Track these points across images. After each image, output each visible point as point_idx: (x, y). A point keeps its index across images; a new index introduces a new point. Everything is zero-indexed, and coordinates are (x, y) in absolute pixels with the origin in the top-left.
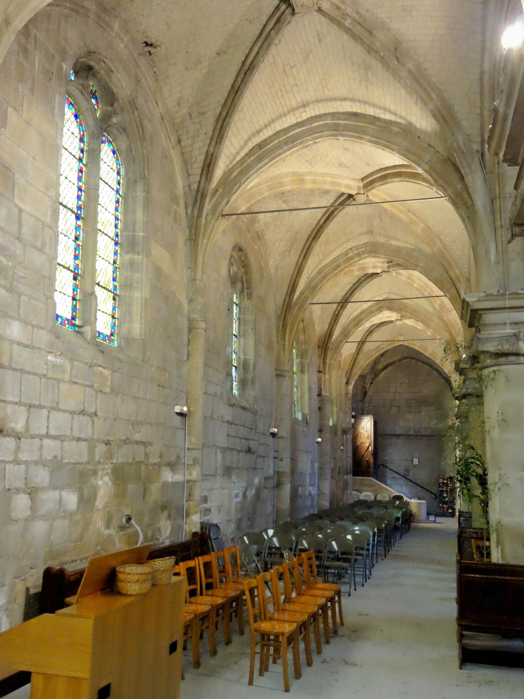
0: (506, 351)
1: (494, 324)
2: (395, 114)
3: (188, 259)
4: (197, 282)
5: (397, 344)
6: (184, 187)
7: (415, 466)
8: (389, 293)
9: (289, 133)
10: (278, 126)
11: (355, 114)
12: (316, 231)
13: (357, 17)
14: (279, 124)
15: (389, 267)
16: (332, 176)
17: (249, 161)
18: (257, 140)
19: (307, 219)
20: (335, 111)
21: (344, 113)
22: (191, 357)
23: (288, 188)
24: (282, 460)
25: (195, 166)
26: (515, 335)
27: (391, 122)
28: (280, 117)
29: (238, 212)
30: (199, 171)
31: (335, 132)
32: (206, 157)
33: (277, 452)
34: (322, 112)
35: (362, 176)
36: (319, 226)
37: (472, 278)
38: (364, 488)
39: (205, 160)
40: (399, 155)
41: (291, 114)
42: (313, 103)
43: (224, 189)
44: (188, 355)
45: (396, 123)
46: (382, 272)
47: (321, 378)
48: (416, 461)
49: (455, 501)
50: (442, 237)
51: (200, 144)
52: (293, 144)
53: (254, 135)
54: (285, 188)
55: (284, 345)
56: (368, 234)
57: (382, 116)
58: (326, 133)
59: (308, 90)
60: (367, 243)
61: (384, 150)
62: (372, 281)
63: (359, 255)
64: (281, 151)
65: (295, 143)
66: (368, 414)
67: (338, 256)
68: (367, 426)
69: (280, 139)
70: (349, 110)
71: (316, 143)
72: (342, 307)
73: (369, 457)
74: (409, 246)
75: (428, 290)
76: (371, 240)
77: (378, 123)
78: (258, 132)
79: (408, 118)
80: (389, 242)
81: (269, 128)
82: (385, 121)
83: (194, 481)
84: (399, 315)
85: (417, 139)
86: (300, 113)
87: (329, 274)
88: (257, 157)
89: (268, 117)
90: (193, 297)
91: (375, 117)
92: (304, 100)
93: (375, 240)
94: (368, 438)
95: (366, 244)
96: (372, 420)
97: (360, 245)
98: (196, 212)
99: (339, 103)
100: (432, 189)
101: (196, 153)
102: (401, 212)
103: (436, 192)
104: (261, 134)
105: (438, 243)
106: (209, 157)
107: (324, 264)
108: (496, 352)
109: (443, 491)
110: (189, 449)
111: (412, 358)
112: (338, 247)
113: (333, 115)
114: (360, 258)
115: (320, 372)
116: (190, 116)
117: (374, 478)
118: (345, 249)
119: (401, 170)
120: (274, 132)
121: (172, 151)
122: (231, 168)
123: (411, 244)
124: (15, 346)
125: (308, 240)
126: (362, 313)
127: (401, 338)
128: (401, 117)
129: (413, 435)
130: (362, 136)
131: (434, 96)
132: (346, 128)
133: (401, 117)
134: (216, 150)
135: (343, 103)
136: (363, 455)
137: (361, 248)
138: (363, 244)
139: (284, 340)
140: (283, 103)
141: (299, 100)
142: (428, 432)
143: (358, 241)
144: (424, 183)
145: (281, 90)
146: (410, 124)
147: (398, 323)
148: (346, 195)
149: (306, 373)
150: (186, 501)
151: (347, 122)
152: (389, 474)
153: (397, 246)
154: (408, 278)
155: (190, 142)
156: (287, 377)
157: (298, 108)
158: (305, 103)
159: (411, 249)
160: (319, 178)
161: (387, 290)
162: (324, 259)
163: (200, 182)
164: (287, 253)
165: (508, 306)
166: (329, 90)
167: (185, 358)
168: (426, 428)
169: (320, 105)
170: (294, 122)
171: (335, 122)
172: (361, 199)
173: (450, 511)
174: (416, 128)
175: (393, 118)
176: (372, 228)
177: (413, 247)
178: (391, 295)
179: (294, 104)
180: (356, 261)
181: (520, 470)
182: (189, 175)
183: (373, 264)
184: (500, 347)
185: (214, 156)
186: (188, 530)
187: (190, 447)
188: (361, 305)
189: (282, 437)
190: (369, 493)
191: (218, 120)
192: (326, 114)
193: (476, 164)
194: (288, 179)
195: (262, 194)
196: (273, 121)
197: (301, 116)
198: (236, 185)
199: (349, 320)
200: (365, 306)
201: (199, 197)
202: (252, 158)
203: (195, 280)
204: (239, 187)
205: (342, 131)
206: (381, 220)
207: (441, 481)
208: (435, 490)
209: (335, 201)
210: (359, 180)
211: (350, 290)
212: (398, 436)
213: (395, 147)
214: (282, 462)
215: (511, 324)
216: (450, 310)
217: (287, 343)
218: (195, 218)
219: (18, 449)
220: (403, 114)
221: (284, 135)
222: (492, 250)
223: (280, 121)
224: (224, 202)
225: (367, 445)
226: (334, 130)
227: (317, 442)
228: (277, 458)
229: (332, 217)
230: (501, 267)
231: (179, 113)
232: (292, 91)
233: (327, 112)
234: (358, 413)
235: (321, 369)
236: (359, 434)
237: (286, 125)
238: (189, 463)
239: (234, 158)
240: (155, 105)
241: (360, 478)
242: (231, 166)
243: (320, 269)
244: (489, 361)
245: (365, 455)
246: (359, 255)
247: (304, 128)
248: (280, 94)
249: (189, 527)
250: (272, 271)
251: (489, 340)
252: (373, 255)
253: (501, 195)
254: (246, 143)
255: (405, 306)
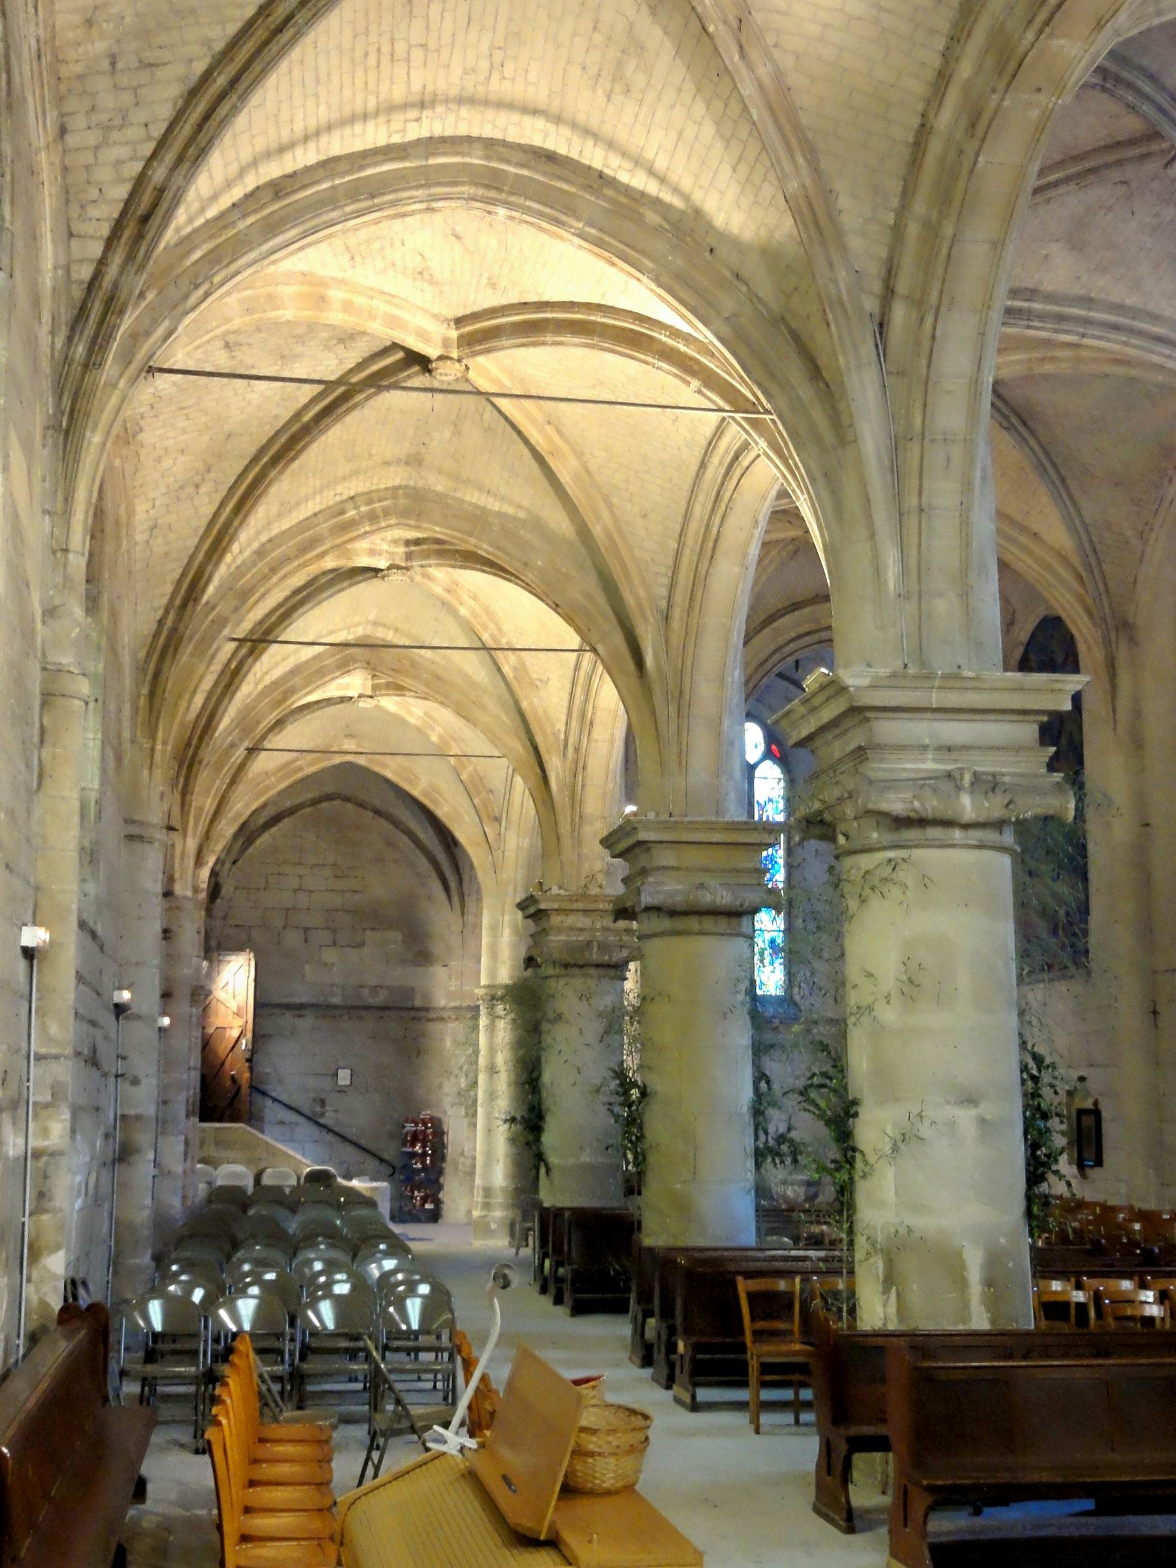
0: (930, 814)
1: (902, 748)
2: (662, 180)
3: (47, 485)
4: (71, 556)
5: (338, 760)
6: (55, 268)
7: (341, 1091)
8: (375, 623)
9: (362, 168)
10: (336, 145)
11: (551, 157)
12: (283, 439)
14: (342, 138)
15: (409, 556)
16: (391, 298)
17: (241, 225)
18: (273, 170)
19: (264, 407)
20: (498, 135)
21: (520, 147)
22: (47, 782)
24: (135, 1082)
25: (94, 212)
26: (949, 775)
27: (640, 197)
28: (352, 120)
30: (105, 230)
31: (492, 194)
32: (132, 194)
33: (124, 1058)
34: (463, 130)
35: (461, 313)
36: (295, 428)
37: (677, 613)
38: (223, 1154)
39: (127, 203)
40: (653, 286)
41: (382, 118)
42: (447, 101)
43: (160, 293)
44: (41, 777)
45: (656, 202)
46: (389, 568)
47: (173, 845)
48: (344, 1078)
49: (441, 1180)
50: (615, 500)
51: (123, 152)
52: (370, 203)
53: (268, 155)
54: (280, 313)
55: (153, 749)
56: (407, 463)
57: (624, 177)
58: (465, 189)
59: (448, 66)
60: (400, 487)
61: (613, 264)
62: (354, 589)
63: (372, 517)
64: (334, 214)
65: (377, 201)
66: (239, 948)
67: (315, 515)
68: (235, 983)
69: (337, 182)
70: (537, 141)
71: (433, 210)
72: (251, 652)
73: (236, 1067)
74: (511, 511)
75: (492, 626)
76: (412, 483)
77: (608, 192)
78: (282, 149)
79: (698, 197)
80: (459, 495)
81: (312, 146)
82: (627, 190)
83: (52, 1154)
84: (369, 683)
85: (707, 254)
86: (406, 121)
88: (264, 218)
89: (323, 114)
90: (57, 602)
91: (601, 175)
92: (430, 88)
93: (420, 484)
94: (238, 1014)
95: (395, 489)
96: (253, 964)
97: (377, 491)
98: (80, 350)
99: (515, 117)
100: (688, 383)
101: (104, 174)
102: (533, 421)
103: (699, 392)
104: (288, 156)
105: (606, 515)
106: (147, 198)
107: (275, 531)
108: (905, 814)
109: (413, 1155)
110: (40, 1058)
111: (347, 799)
112: (321, 492)
113: (490, 145)
114: (375, 527)
116: (113, 64)
118: (338, 498)
119: (593, 318)
120: (323, 157)
121: (43, 156)
122: (188, 237)
123: (519, 506)
125: (255, 459)
126: (294, 672)
127: (350, 745)
128: (676, 190)
129: (342, 1007)
130: (563, 218)
132: (520, 188)
133: (676, 190)
134: (178, 180)
135: (528, 120)
136: (223, 1064)
137: (379, 501)
138: (387, 489)
139: (153, 737)
140: (371, 87)
141: (416, 86)
142: (381, 999)
143: (375, 480)
144: (661, 364)
145: (379, 50)
146: (698, 213)
147: (364, 704)
148: (400, 355)
150: (31, 1214)
151: (525, 172)
152: (272, 1112)
153: (477, 506)
154: (449, 591)
155: (92, 138)
156: (157, 844)
157: (405, 106)
158: (427, 98)
159: (515, 518)
160: (359, 300)
161: (372, 617)
162: (280, 516)
163: (102, 262)
164: (190, 490)
165: (934, 706)
166: (527, 82)
168: (376, 989)
169: (464, 112)
170: (382, 141)
171: (494, 164)
172: (447, 373)
173: (429, 1206)
174: (710, 226)
175: (652, 188)
176: (423, 450)
177: (521, 514)
178: (380, 629)
179: (398, 94)
180: (366, 533)
181: (948, 1103)
182: (71, 235)
183: (376, 547)
184: (916, 804)
185: (168, 195)
186: (35, 1299)
187: (43, 1051)
188: (295, 652)
189: (139, 1017)
190: (239, 1168)
191: (193, 93)
192: (469, 139)
193: (867, 348)
195: (227, 320)
196: (329, 128)
197: (404, 130)
198: (197, 286)
199: (260, 687)
200: (308, 653)
201: (96, 309)
202: (250, 220)
203: (66, 551)
204: (207, 295)
205: (511, 194)
206: (457, 433)
207: (410, 1127)
208: (390, 1151)
209: (360, 367)
210: (448, 321)
211: (280, 605)
212: (298, 1009)
213: (648, 263)
214: (132, 1088)
215: (939, 748)
216: (537, 683)
217: (159, 747)
218: (76, 369)
220: (686, 184)
221: (349, 172)
222: (891, 562)
223: (347, 131)
224: (160, 332)
225: (235, 1033)
226: (488, 187)
228: (122, 1075)
229: (344, 408)
230: (911, 607)
231: (81, 50)
232: (408, 60)
233: (475, 133)
234: (215, 947)
235: (175, 823)
236: (214, 1002)
237: (358, 146)
238: (40, 1099)
240: (31, 10)
241: (217, 1125)
242: (189, 229)
243: (263, 545)
244: (875, 835)
245: (227, 1064)
247: (408, 164)
248: (372, 59)
249: (37, 1291)
250: (140, 537)
251: (891, 784)
252: (412, 522)
253: (927, 434)
254: (242, 173)
255: (414, 664)
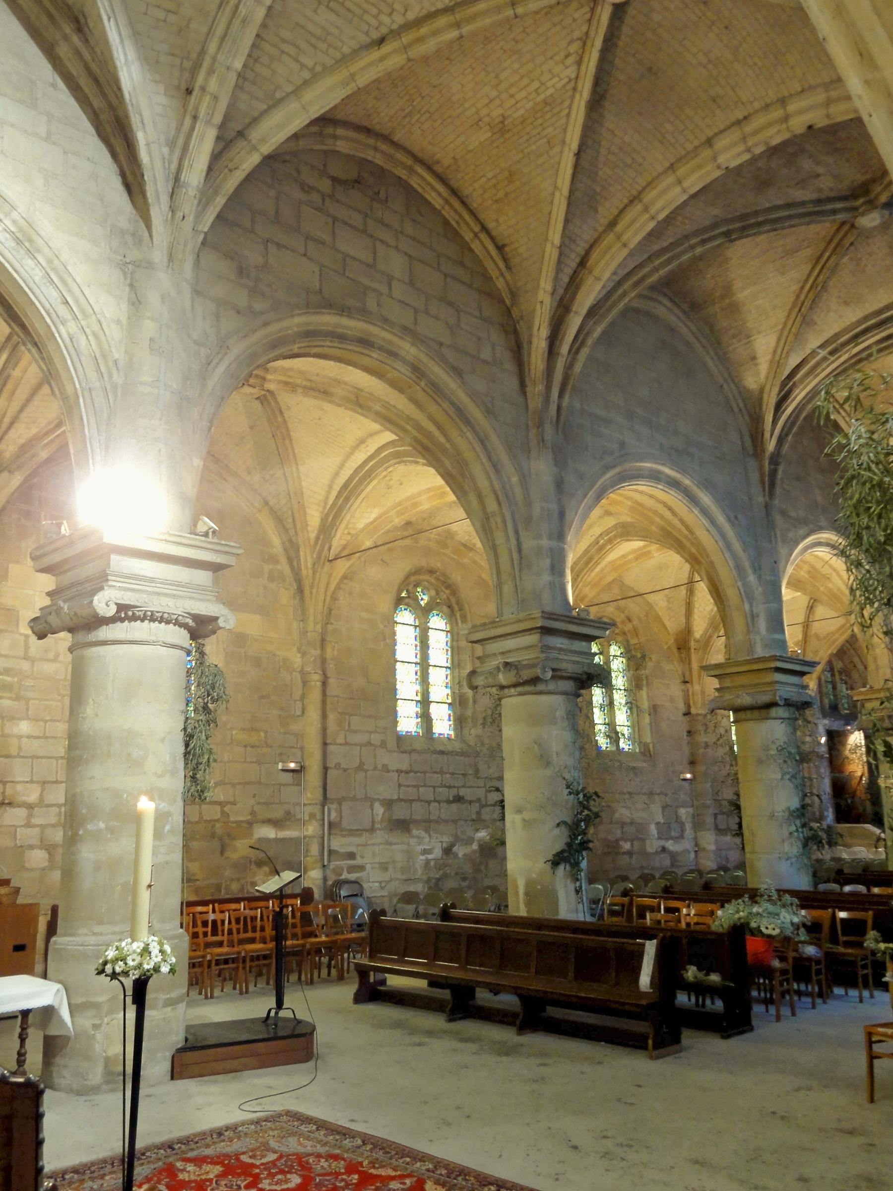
13: (308, 384)
23: (426, 506)
29: (363, 548)
87: (583, 569)
95: (615, 527)
105: (657, 519)
115: (685, 682)
117: (874, 825)
124: (24, 740)
131: (410, 428)
149: (645, 688)
167: (298, 713)
192: (388, 444)
194: (424, 497)
219: (30, 816)
227: (685, 780)
239: (326, 503)
246: (610, 541)
